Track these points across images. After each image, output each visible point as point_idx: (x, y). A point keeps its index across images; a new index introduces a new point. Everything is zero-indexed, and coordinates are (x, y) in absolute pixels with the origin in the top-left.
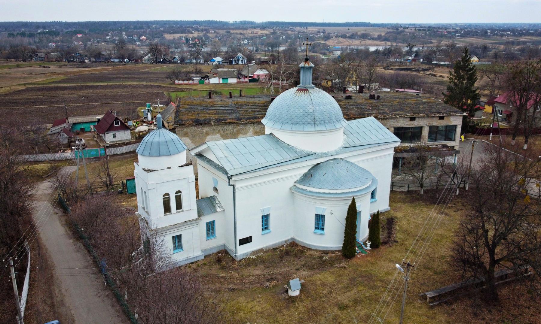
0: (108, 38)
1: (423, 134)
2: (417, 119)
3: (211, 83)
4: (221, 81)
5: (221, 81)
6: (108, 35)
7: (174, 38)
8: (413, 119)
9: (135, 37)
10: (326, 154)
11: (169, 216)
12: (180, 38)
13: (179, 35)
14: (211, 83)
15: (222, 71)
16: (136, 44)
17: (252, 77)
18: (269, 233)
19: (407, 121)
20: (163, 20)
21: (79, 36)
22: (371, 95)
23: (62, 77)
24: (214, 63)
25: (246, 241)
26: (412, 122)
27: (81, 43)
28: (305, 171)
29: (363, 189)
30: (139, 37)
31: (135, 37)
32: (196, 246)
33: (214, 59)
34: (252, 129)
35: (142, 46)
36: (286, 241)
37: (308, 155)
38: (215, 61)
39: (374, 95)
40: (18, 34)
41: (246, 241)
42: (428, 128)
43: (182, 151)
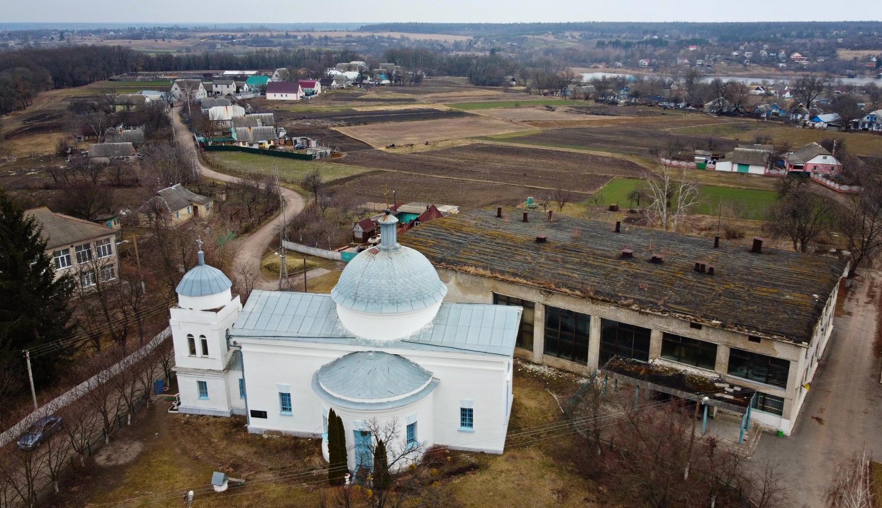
0: (735, 53)
1: (718, 358)
2: (704, 329)
3: (717, 169)
4: (736, 168)
5: (736, 168)
6: (735, 50)
7: (856, 59)
8: (698, 327)
9: (782, 54)
10: (368, 343)
11: (193, 359)
12: (868, 59)
13: (867, 53)
14: (717, 169)
15: (742, 152)
16: (777, 67)
17: (801, 167)
18: (470, 432)
19: (686, 328)
20: (864, 20)
21: (691, 49)
22: (697, 264)
23: (537, 130)
24: (817, 125)
25: (262, 415)
26: (694, 331)
27: (686, 61)
28: (340, 356)
29: (350, 402)
30: (788, 55)
31: (782, 54)
32: (219, 402)
33: (820, 116)
34: (454, 278)
35: (788, 70)
36: (314, 435)
37: (344, 337)
38: (819, 121)
39: (703, 266)
40: (610, 42)
41: (262, 415)
42: (728, 351)
43: (225, 290)
